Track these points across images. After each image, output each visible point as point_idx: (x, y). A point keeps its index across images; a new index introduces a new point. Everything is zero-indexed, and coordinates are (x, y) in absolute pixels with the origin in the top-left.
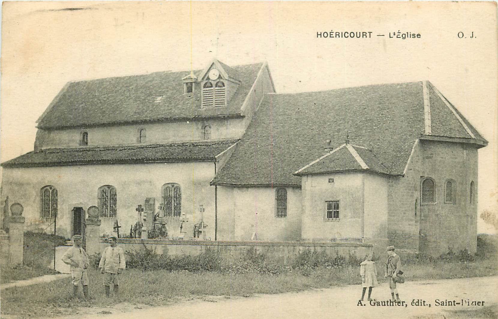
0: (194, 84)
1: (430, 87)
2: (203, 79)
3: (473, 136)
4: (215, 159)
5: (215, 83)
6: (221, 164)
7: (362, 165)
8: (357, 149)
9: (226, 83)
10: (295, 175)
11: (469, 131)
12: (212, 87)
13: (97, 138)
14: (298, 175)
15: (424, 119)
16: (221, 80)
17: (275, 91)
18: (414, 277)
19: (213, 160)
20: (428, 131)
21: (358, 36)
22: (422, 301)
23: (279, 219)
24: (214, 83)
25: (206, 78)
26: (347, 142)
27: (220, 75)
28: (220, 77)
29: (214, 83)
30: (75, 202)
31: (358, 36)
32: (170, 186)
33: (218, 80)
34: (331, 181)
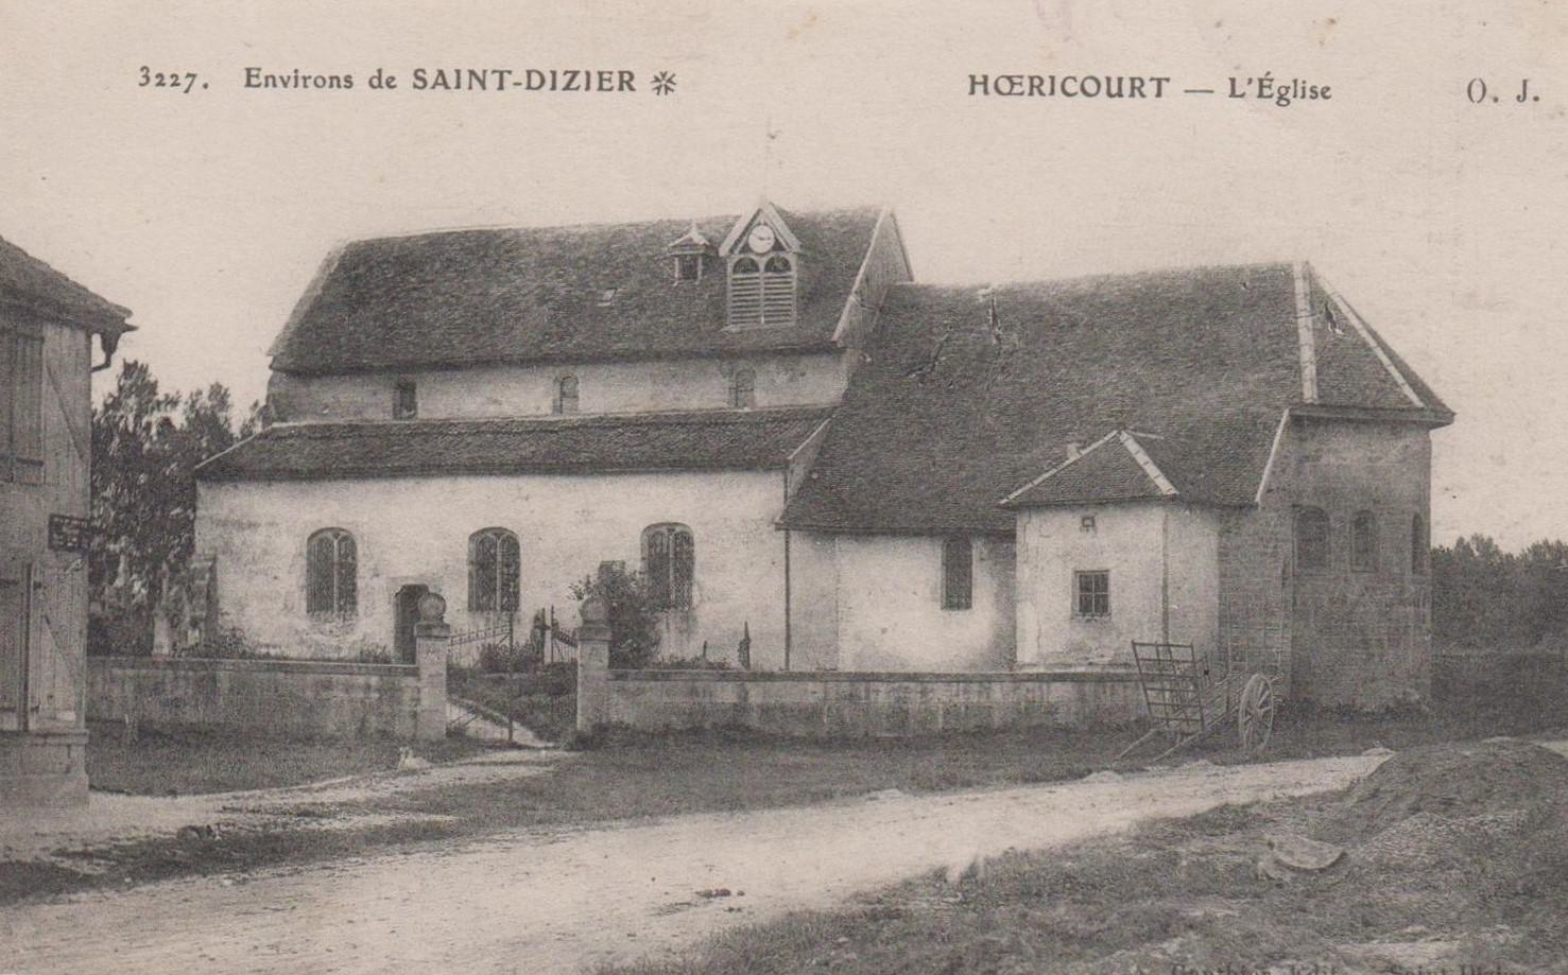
0: (700, 261)
1: (1310, 277)
2: (731, 251)
3: (1418, 403)
4: (787, 463)
5: (765, 259)
6: (798, 473)
7: (1161, 487)
8: (1139, 441)
9: (792, 260)
10: (999, 506)
11: (1408, 391)
12: (757, 270)
13: (454, 402)
14: (1007, 507)
15: (1296, 330)
16: (782, 254)
17: (911, 279)
18: (1350, 421)
19: (784, 466)
20: (1309, 393)
21: (1114, 90)
22: (1308, 86)
23: (47, 517)
24: (762, 263)
25: (741, 245)
26: (1122, 427)
27: (777, 240)
28: (778, 247)
29: (762, 263)
30: (408, 570)
31: (1114, 90)
32: (664, 530)
33: (772, 255)
34: (1088, 522)
